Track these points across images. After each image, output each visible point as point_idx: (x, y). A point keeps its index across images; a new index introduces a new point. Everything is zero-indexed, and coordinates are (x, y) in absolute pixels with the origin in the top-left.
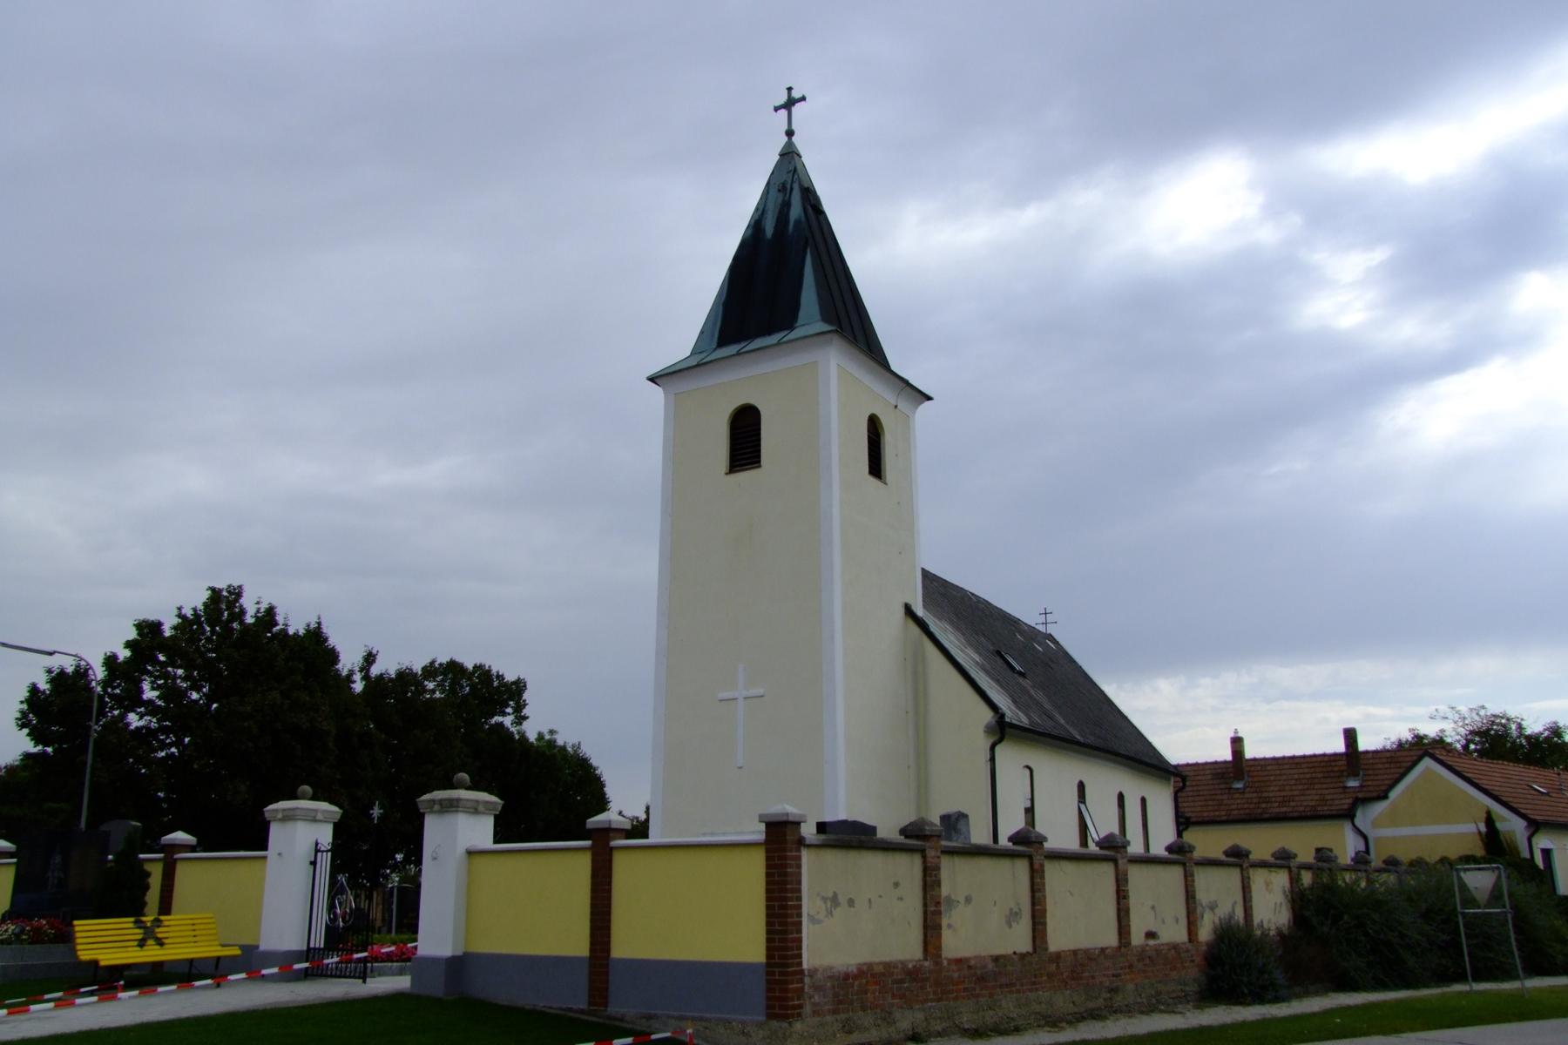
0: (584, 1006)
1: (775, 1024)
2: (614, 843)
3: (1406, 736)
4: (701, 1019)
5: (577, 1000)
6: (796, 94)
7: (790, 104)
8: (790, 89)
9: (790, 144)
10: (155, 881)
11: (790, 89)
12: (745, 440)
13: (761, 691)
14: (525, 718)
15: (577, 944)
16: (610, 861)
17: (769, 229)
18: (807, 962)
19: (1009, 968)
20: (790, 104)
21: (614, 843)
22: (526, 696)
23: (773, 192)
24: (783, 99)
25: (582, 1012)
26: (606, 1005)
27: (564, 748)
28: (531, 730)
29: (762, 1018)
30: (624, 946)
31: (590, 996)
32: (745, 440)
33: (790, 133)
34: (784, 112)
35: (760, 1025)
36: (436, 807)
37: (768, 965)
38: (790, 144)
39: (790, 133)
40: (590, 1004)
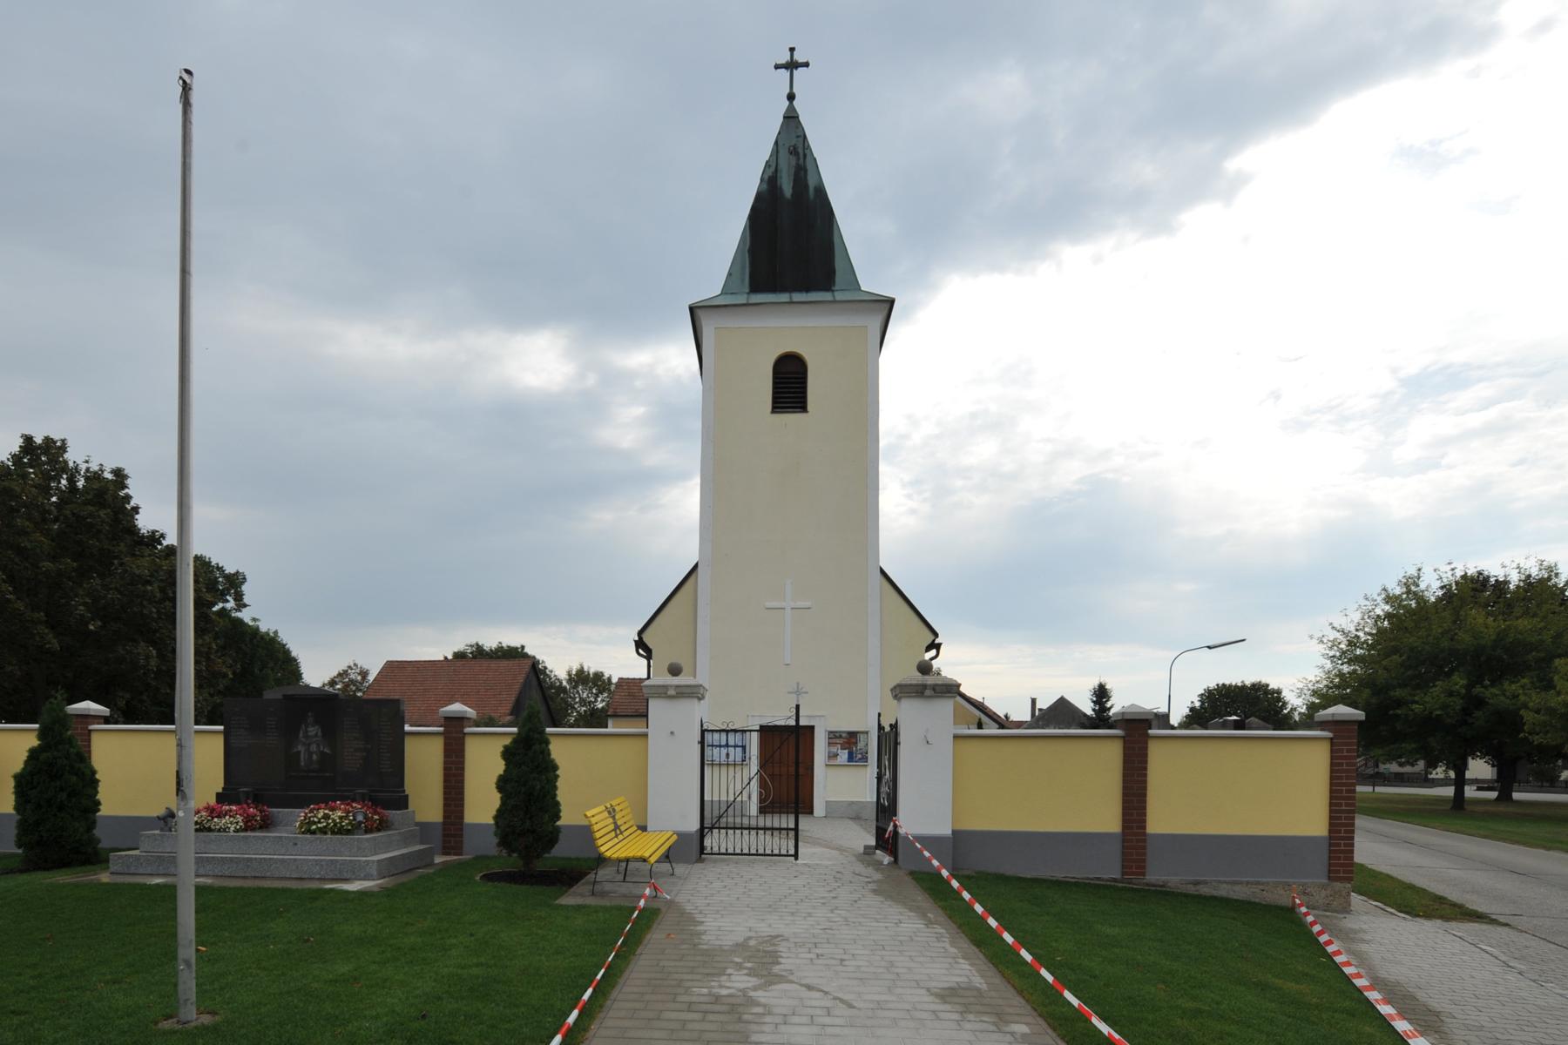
0: (1118, 876)
1: (1338, 885)
2: (467, 730)
3: (1273, 685)
4: (1258, 883)
5: (1109, 868)
6: (799, 57)
7: (792, 66)
8: (792, 50)
9: (791, 108)
10: (1408, 769)
11: (792, 50)
12: (790, 385)
13: (807, 604)
14: (245, 606)
15: (1106, 819)
16: (1146, 749)
17: (787, 189)
18: (105, 810)
19: (360, 818)
20: (792, 66)
21: (467, 730)
22: (244, 588)
23: (783, 153)
24: (785, 58)
25: (1115, 880)
26: (1144, 874)
27: (267, 634)
28: (245, 616)
29: (1326, 881)
30: (1159, 822)
31: (1123, 867)
32: (790, 385)
33: (791, 97)
34: (785, 73)
35: (1324, 887)
36: (928, 692)
37: (444, 823)
38: (791, 108)
39: (791, 97)
40: (1123, 874)
